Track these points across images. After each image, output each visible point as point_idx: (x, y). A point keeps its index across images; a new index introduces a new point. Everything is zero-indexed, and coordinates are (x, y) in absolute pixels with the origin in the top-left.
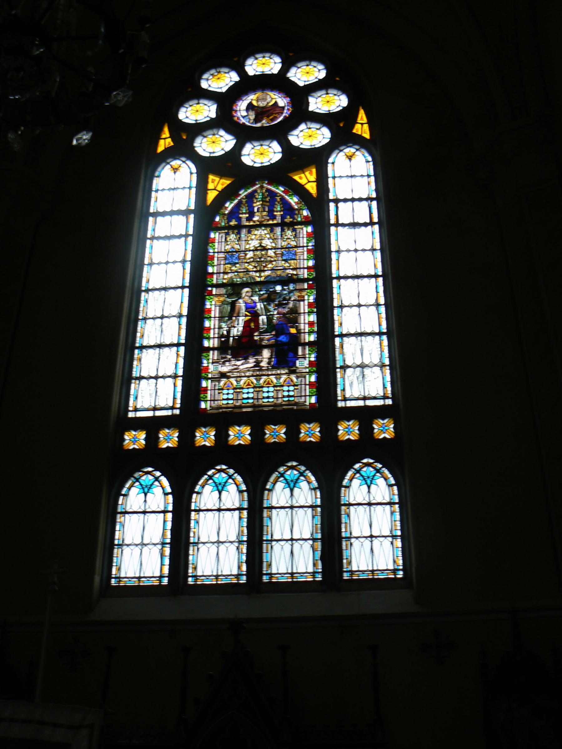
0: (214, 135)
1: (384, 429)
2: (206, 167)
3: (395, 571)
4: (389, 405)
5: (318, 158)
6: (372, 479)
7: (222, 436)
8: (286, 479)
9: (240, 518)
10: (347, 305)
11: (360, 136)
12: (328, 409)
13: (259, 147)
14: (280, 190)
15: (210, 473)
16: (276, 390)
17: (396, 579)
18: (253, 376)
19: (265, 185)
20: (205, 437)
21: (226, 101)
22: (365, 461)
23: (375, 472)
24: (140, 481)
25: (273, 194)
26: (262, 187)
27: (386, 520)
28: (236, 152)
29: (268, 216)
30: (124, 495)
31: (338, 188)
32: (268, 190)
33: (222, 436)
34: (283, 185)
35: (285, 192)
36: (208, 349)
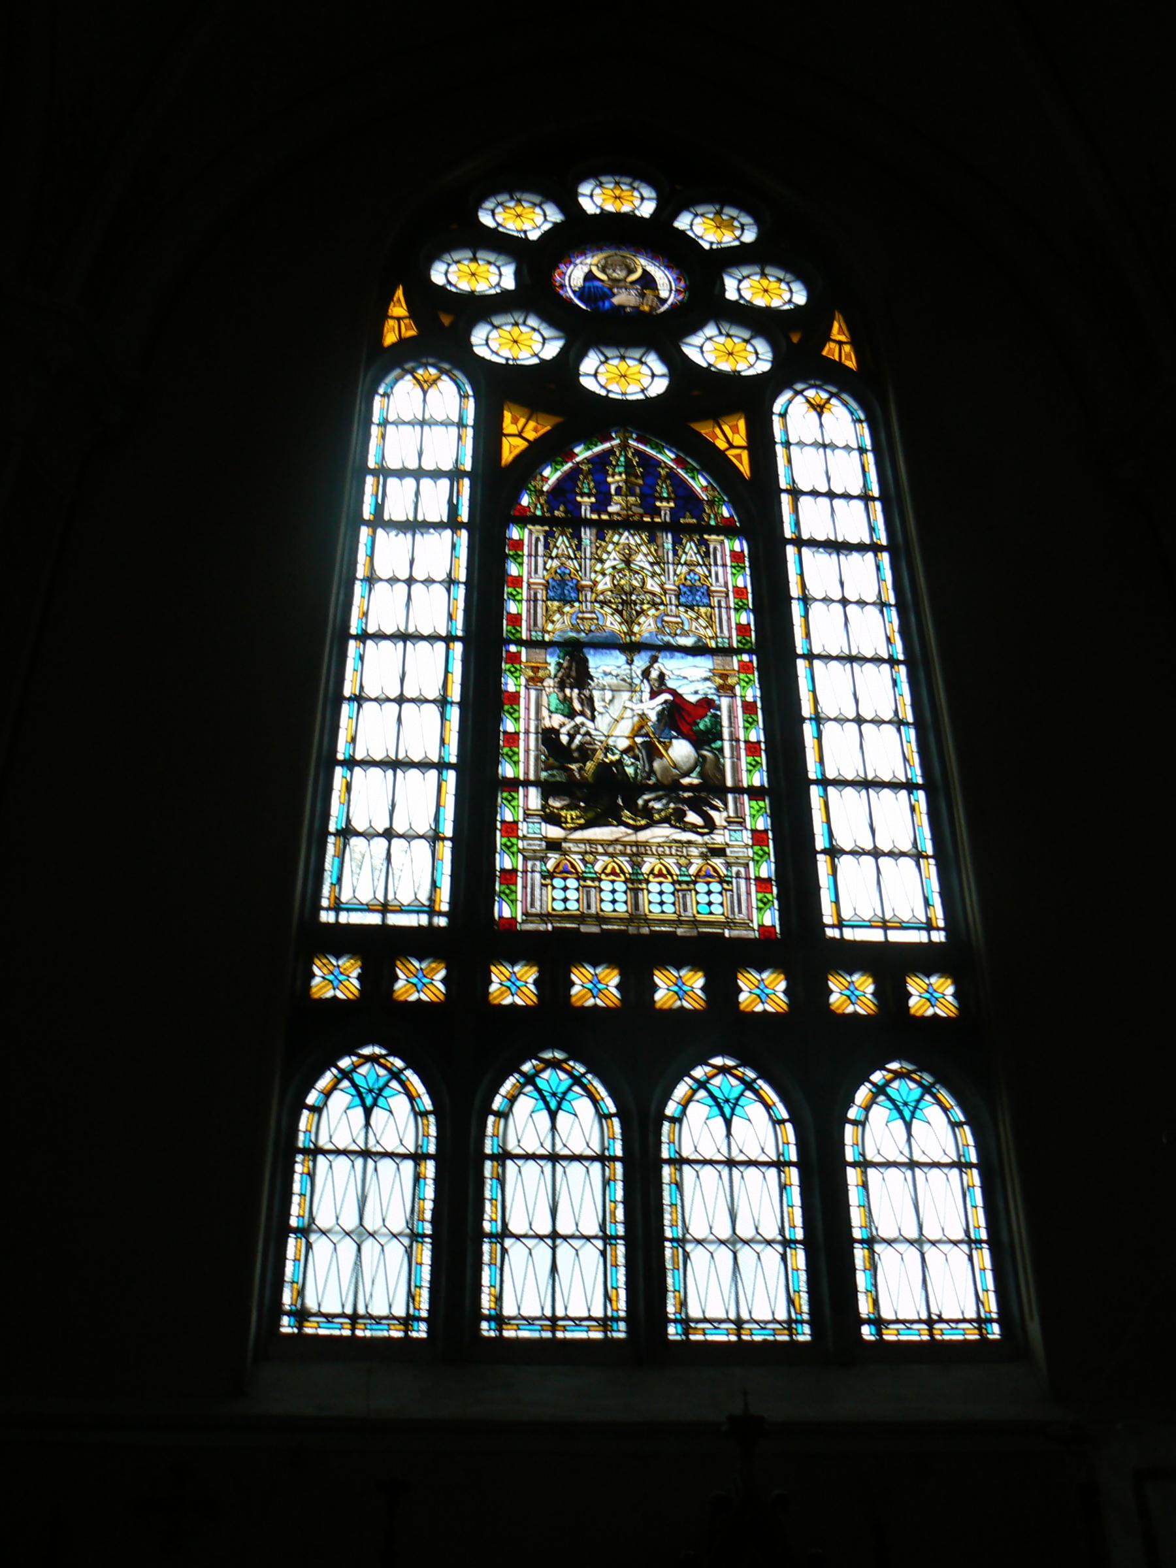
0: (516, 324)
1: (932, 996)
2: (497, 387)
3: (605, 1323)
4: (439, 927)
5: (751, 399)
6: (916, 1108)
7: (553, 985)
8: (539, 1091)
9: (783, 1187)
10: (373, 697)
11: (839, 365)
12: (804, 944)
13: (616, 362)
14: (667, 457)
15: (527, 1067)
16: (584, 887)
17: (793, 1343)
18: (623, 854)
19: (631, 442)
20: (513, 985)
21: (537, 261)
22: (367, 1051)
23: (742, 1087)
24: (538, 1081)
25: (650, 464)
26: (624, 446)
27: (951, 1203)
28: (567, 363)
29: (640, 506)
30: (673, 1120)
31: (801, 467)
32: (637, 452)
33: (553, 985)
34: (673, 444)
35: (677, 461)
36: (513, 785)
